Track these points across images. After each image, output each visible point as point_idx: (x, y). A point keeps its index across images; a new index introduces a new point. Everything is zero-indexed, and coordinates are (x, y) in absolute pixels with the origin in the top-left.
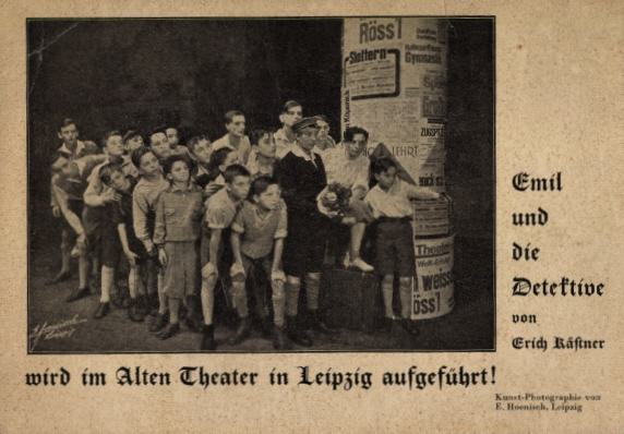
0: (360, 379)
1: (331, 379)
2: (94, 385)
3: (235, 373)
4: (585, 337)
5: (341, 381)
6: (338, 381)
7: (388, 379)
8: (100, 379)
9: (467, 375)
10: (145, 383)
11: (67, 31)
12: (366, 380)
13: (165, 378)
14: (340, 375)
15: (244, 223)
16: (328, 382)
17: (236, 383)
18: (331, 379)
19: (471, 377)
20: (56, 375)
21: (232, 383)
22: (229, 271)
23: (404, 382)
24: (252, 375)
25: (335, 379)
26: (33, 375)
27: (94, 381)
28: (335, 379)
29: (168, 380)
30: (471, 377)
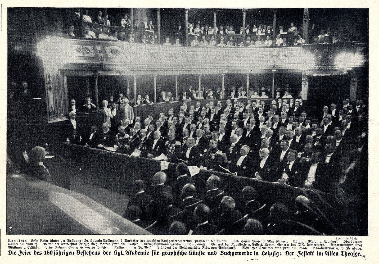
0: (276, 254)
1: (269, 254)
2: (142, 255)
3: (354, 253)
4: (64, 256)
5: (272, 254)
6: (271, 254)
7: (159, 241)
8: (321, 254)
9: (61, 252)
10: (332, 255)
11: (97, 86)
12: (119, 254)
13: (73, 253)
14: (271, 253)
15: (127, 35)
16: (268, 255)
17: (131, 254)
18: (269, 254)
19: (61, 253)
20: (63, 252)
21: (310, 255)
22: (213, 92)
23: (319, 253)
24: (30, 252)
25: (270, 254)
26: (239, 252)
27: (320, 254)
28: (270, 254)
29: (338, 254)
30: (61, 253)
